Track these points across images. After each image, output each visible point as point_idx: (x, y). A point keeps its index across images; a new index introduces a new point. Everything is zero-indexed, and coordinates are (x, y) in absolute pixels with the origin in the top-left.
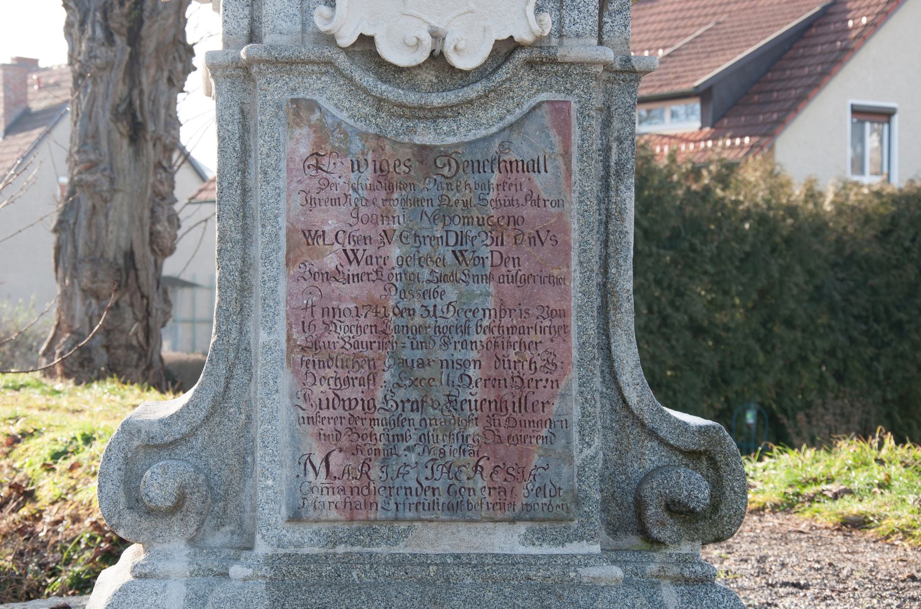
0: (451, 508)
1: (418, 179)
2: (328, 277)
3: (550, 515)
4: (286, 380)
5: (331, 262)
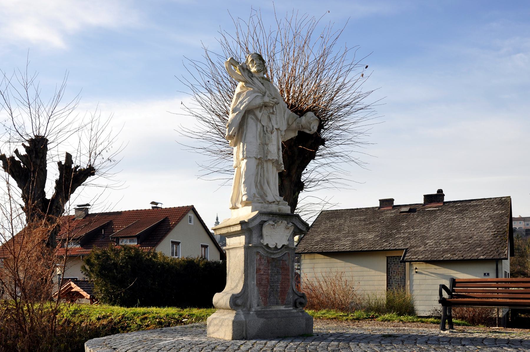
0: (277, 304)
1: (272, 262)
2: (262, 274)
3: (286, 305)
4: (256, 288)
5: (262, 273)
